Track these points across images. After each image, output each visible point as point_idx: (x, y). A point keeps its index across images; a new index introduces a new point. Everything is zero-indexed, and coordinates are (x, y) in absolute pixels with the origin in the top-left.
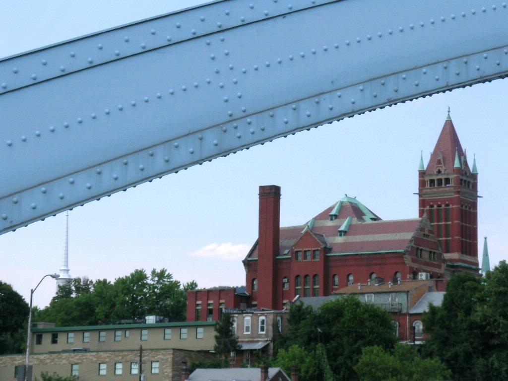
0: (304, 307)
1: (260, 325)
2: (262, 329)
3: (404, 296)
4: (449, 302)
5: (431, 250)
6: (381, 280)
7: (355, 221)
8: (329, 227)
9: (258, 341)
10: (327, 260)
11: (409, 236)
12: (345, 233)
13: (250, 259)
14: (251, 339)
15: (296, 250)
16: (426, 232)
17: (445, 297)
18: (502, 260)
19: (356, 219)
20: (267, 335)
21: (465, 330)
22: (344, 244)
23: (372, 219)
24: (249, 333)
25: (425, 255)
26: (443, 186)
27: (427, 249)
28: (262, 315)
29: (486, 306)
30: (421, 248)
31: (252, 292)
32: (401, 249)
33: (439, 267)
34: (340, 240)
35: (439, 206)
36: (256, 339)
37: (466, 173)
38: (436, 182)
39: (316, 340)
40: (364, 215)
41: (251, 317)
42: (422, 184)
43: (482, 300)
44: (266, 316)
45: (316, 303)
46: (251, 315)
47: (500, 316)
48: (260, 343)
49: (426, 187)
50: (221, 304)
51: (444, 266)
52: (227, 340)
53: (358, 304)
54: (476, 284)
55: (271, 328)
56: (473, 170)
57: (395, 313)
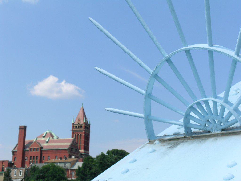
0: (36, 167)
1: (22, 173)
2: (21, 174)
3: (69, 164)
4: (84, 166)
5: (76, 149)
6: (61, 158)
7: (51, 138)
8: (42, 140)
9: (19, 179)
10: (41, 151)
11: (69, 144)
12: (48, 142)
13: (14, 150)
14: (16, 178)
15: (31, 148)
16: (75, 143)
17: (83, 164)
18: (102, 152)
19: (51, 138)
20: (22, 177)
21: (89, 175)
22: (47, 146)
23: (57, 138)
24: (16, 176)
25: (74, 150)
26: (80, 128)
27: (75, 148)
28: (21, 169)
29: (96, 167)
30: (72, 148)
31: (14, 162)
32: (66, 148)
33: (78, 154)
34: (46, 144)
35: (78, 134)
36: (18, 178)
37: (87, 124)
38: (77, 127)
39: (40, 178)
40: (54, 136)
41: (17, 170)
42: (73, 127)
43: (94, 165)
44: (22, 170)
45: (40, 166)
46: (17, 169)
47: (101, 170)
48: (19, 179)
49: (74, 128)
50: (3, 166)
51: (79, 154)
52: (8, 178)
53: (55, 166)
54: (93, 160)
55: (24, 174)
56: (89, 123)
57: (66, 169)
